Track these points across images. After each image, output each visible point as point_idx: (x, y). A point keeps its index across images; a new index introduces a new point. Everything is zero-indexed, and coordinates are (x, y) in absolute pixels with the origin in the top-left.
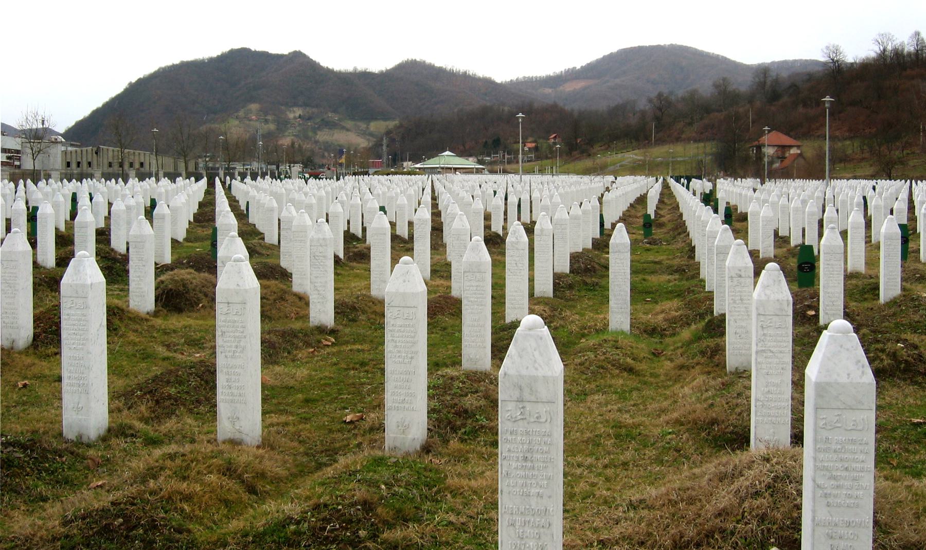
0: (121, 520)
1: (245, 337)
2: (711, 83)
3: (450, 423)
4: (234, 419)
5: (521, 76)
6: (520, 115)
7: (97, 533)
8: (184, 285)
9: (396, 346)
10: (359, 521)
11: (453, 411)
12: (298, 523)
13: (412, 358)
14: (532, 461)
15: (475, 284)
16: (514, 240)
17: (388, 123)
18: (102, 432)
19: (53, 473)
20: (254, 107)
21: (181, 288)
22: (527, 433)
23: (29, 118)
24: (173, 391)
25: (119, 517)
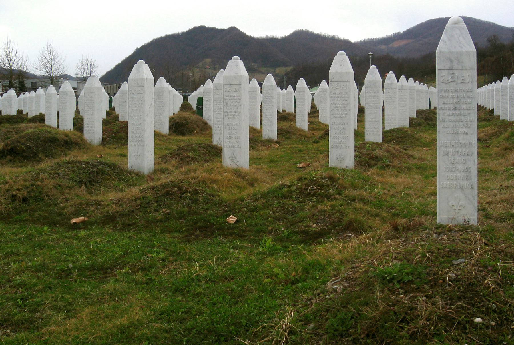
0: (176, 189)
1: (241, 105)
2: (486, 39)
3: (367, 162)
4: (233, 158)
5: (366, 38)
6: (370, 53)
7: (162, 196)
8: (186, 120)
9: (336, 107)
10: (328, 186)
11: (369, 157)
12: (289, 187)
13: (346, 114)
14: (459, 110)
15: (372, 94)
16: (389, 82)
17: (287, 68)
18: (151, 171)
19: (127, 181)
20: (208, 60)
21: (184, 122)
22: (456, 91)
23: (84, 63)
24: (190, 154)
25: (175, 187)
